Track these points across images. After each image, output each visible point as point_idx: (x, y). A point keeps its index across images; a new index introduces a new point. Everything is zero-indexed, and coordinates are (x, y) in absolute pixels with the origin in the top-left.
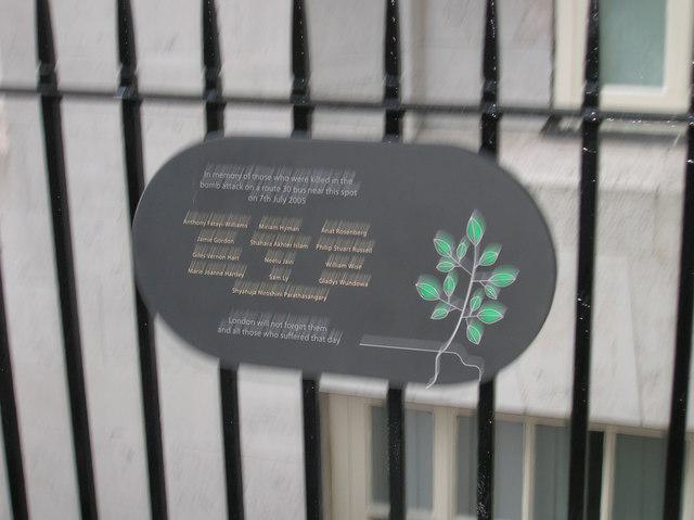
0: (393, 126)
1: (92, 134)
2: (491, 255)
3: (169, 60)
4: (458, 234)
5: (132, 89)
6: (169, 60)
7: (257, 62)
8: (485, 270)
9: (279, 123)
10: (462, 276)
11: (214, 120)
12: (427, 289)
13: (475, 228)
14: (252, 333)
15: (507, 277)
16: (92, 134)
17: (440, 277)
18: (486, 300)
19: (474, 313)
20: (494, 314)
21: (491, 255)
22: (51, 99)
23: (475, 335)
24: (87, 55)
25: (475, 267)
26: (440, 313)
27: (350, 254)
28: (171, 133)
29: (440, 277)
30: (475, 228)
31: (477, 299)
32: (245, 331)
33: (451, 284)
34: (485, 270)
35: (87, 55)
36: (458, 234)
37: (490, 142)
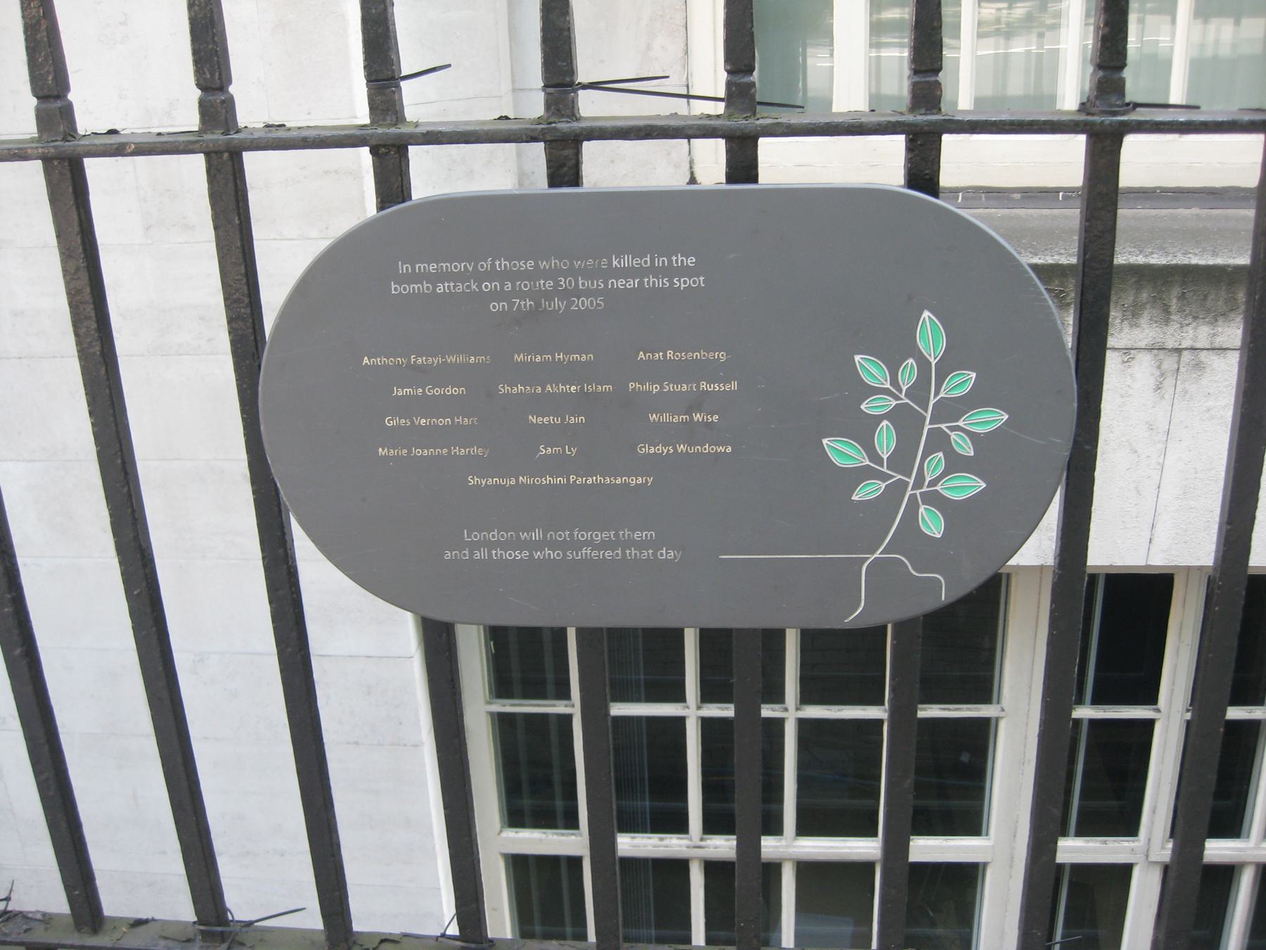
0: (565, 170)
1: (153, 225)
2: (962, 383)
3: (298, 66)
4: (897, 347)
5: (875, 16)
6: (298, 66)
7: (468, 62)
8: (951, 410)
9: (511, 171)
10: (905, 421)
11: (392, 184)
12: (842, 452)
13: (931, 336)
14: (510, 555)
15: (989, 420)
16: (153, 225)
17: (863, 432)
18: (956, 464)
19: (933, 483)
20: (964, 487)
21: (962, 383)
22: (688, 97)
23: (932, 524)
24: (130, 74)
25: (932, 402)
26: (867, 491)
27: (697, 402)
28: (308, 210)
29: (863, 432)
30: (931, 336)
31: (936, 463)
32: (496, 553)
33: (886, 440)
34: (951, 410)
35: (130, 74)
36: (897, 347)
37: (923, 173)
